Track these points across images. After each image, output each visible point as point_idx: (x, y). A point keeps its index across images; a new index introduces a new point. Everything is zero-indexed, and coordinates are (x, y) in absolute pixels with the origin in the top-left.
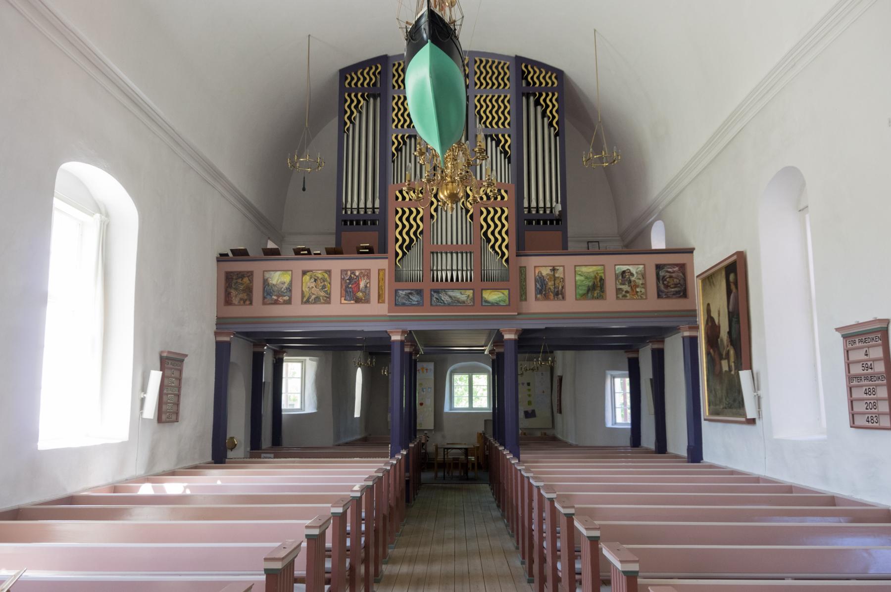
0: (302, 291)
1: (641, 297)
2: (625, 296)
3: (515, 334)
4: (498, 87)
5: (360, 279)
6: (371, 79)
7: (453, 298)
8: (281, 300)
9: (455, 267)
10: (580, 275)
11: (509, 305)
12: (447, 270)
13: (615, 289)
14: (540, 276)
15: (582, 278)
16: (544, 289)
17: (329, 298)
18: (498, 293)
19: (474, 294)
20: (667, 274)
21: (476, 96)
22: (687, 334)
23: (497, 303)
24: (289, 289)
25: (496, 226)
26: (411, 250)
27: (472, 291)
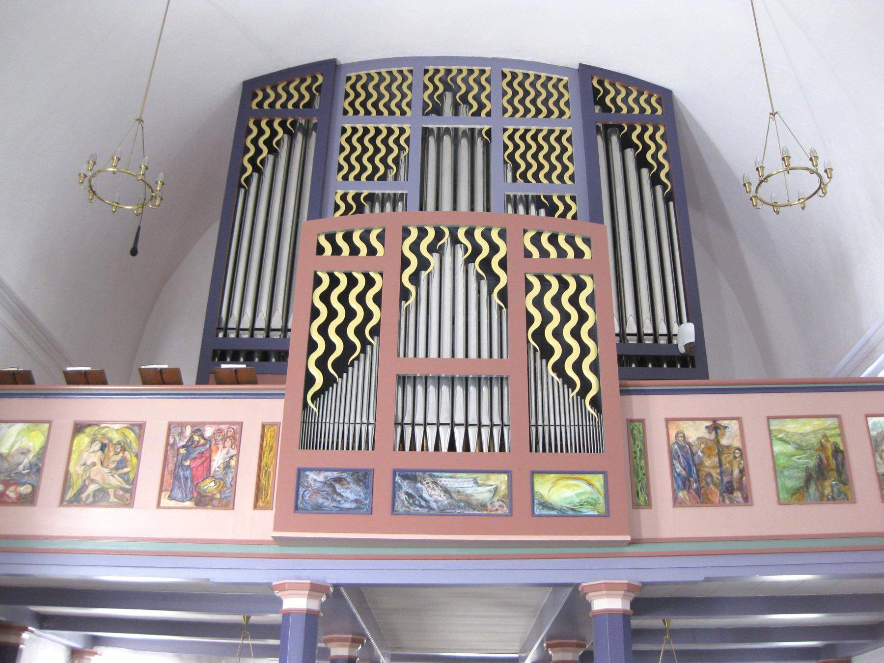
0: (67, 472)
3: (624, 597)
5: (213, 448)
7: (454, 495)
8: (11, 493)
9: (459, 418)
10: (781, 439)
11: (607, 514)
12: (439, 424)
14: (682, 443)
15: (790, 449)
16: (694, 476)
17: (132, 492)
23: (573, 510)
24: (37, 468)
25: (566, 317)
26: (347, 372)
27: (505, 477)
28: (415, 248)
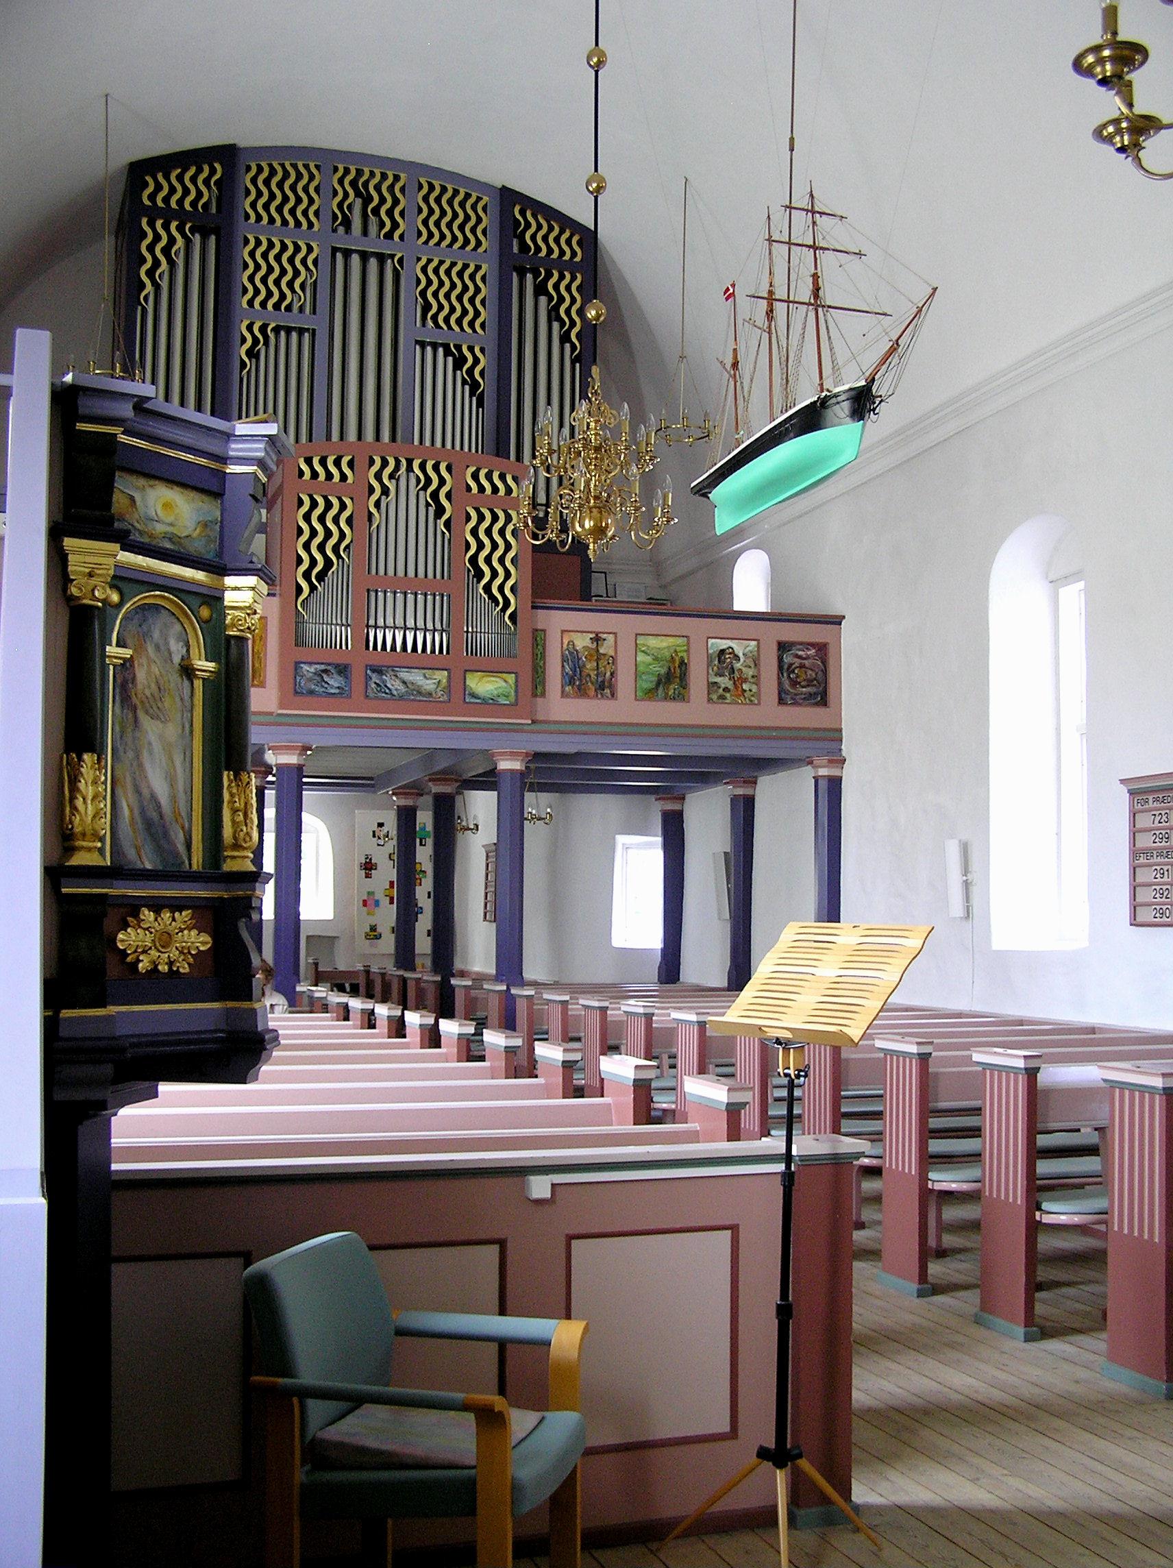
1: (751, 701)
2: (722, 697)
4: (463, 247)
6: (200, 194)
7: (410, 686)
10: (643, 651)
13: (706, 683)
14: (572, 650)
16: (578, 676)
18: (498, 679)
19: (449, 677)
20: (797, 660)
21: (419, 259)
22: (823, 772)
26: (324, 581)
28: (378, 476)
